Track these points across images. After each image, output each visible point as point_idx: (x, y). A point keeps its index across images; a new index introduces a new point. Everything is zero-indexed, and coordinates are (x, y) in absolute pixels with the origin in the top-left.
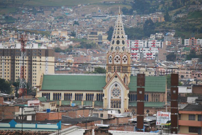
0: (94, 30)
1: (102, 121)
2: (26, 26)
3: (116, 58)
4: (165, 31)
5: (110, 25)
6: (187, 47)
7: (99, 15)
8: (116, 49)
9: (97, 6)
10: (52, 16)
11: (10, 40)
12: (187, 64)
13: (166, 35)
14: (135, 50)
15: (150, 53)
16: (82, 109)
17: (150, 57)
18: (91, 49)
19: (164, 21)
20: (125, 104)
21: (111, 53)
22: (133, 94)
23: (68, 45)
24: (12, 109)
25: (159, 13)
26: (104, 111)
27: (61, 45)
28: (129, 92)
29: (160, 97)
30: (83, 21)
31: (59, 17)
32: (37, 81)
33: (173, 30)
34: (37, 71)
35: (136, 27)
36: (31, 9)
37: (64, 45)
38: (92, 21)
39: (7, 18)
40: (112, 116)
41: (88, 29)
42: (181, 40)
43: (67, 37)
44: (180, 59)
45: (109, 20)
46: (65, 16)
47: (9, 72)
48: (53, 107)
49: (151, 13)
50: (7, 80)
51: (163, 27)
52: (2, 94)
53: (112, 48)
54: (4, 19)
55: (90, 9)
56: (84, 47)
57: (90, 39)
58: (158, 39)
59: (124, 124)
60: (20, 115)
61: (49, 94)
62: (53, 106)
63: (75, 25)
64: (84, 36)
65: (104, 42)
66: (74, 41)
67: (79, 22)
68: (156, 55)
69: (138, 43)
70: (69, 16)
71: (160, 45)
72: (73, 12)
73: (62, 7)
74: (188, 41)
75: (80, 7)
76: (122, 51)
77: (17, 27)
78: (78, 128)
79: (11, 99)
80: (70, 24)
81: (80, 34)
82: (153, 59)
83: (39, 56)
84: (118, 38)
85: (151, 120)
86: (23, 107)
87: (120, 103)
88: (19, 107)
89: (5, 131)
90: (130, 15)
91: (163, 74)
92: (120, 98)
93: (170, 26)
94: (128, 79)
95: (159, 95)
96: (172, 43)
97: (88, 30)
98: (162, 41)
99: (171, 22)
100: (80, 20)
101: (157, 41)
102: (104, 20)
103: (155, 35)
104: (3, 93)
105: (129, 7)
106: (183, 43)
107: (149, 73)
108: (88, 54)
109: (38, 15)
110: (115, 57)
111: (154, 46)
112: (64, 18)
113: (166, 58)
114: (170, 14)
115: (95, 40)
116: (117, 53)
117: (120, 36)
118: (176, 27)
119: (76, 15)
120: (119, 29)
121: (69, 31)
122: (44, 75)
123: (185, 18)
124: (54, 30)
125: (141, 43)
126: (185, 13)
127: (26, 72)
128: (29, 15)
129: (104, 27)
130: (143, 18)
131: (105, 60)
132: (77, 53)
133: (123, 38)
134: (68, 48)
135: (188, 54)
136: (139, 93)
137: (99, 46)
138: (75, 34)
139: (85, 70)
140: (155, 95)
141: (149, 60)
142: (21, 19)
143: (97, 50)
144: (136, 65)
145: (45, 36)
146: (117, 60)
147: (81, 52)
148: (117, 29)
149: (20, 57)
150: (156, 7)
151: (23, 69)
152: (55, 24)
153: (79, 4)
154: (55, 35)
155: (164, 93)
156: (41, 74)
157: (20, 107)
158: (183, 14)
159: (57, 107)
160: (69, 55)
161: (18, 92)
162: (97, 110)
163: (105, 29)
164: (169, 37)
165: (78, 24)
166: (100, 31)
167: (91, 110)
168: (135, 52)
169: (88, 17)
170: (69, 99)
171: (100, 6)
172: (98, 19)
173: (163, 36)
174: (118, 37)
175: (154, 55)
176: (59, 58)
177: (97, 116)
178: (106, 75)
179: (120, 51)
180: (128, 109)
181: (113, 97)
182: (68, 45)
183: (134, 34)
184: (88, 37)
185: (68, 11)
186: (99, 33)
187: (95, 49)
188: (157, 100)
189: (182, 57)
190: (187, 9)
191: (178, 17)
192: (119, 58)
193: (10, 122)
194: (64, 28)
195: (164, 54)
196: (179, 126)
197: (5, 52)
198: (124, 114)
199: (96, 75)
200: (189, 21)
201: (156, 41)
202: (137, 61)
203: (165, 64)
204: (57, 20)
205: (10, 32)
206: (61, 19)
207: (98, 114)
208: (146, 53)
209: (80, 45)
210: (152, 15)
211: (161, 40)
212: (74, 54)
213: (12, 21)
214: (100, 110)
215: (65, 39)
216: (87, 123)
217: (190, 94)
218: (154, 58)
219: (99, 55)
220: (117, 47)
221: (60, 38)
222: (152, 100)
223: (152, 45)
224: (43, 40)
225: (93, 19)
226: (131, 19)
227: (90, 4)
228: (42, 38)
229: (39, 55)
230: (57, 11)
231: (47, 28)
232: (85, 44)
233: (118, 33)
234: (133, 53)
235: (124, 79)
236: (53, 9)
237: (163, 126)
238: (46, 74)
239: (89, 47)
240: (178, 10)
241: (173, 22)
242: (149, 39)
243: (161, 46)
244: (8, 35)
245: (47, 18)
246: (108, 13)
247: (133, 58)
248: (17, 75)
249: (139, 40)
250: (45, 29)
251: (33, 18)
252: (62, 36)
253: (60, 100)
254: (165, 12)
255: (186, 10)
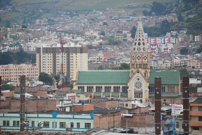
0: (120, 29)
1: (127, 110)
2: (65, 27)
3: (138, 57)
4: (179, 29)
5: (134, 25)
6: (197, 42)
7: (124, 17)
8: (138, 50)
9: (122, 9)
10: (86, 18)
11: (52, 39)
12: (197, 57)
13: (180, 32)
14: (154, 46)
15: (166, 48)
16: (110, 100)
17: (166, 52)
18: (118, 46)
19: (178, 21)
20: (146, 95)
21: (133, 53)
22: (152, 86)
23: (99, 42)
24: (54, 102)
25: (173, 14)
26: (129, 102)
27: (93, 43)
28: (149, 85)
29: (174, 88)
30: (111, 22)
31: (91, 19)
32: (74, 77)
33: (185, 29)
34: (73, 65)
35: (154, 26)
36: (69, 13)
37: (95, 43)
38: (118, 22)
39: (49, 20)
40: (135, 105)
41: (115, 28)
42: (192, 37)
43: (98, 36)
44: (191, 53)
45: (132, 21)
46: (96, 18)
47: (51, 61)
48: (86, 98)
49: (167, 14)
50: (50, 74)
51: (177, 26)
52: (46, 86)
53: (134, 49)
54: (47, 22)
55: (117, 11)
56: (111, 44)
57: (116, 37)
58: (173, 36)
59: (145, 113)
60: (60, 107)
61: (84, 87)
62: (86, 97)
63: (104, 25)
64: (112, 35)
65: (128, 40)
66: (103, 39)
67: (107, 23)
68: (172, 50)
69: (156, 40)
70: (99, 18)
71: (174, 41)
72: (102, 15)
73: (94, 11)
74: (198, 37)
75: (108, 10)
76: (143, 51)
77: (58, 28)
78: (106, 132)
79: (53, 92)
80: (101, 24)
81: (109, 33)
82: (169, 53)
83: (75, 53)
84: (139, 41)
85: (168, 109)
86: (62, 101)
87: (142, 94)
88: (59, 100)
89: (47, 133)
90: (150, 16)
91: (178, 66)
92: (142, 89)
93: (183, 25)
94: (148, 74)
95: (174, 87)
96: (184, 39)
97: (115, 29)
98: (176, 38)
99: (184, 22)
100: (109, 21)
101: (172, 38)
102: (129, 21)
103: (170, 33)
104: (47, 85)
105: (148, 10)
106: (194, 39)
107: (166, 65)
108: (115, 50)
109: (74, 18)
111: (169, 42)
112: (95, 19)
113: (180, 52)
114: (182, 15)
115: (121, 38)
116: (139, 53)
117: (140, 39)
118: (188, 26)
119: (105, 17)
120: (140, 33)
121: (100, 30)
122: (79, 71)
123: (195, 18)
124: (87, 30)
125: (159, 40)
126: (195, 14)
127: (65, 69)
128: (67, 18)
129: (128, 27)
130: (160, 19)
131: (129, 54)
132: (107, 49)
133: (144, 40)
134: (99, 45)
135: (198, 48)
136: (156, 93)
137: (124, 43)
138: (105, 33)
139: (113, 63)
140: (170, 87)
141: (166, 54)
142: (60, 21)
143: (122, 46)
144: (155, 58)
145: (80, 35)
147: (109, 48)
148: (138, 33)
149: (60, 54)
150: (171, 9)
151: (62, 69)
152: (88, 25)
153: (108, 8)
154: (88, 35)
155: (178, 85)
156: (77, 71)
157: (60, 101)
158: (193, 15)
159: (90, 98)
160: (100, 51)
161: (59, 84)
162: (122, 101)
163: (129, 28)
164: (182, 34)
165: (107, 25)
166: (125, 30)
167: (118, 101)
168: (154, 47)
169: (115, 18)
170: (100, 91)
171: (125, 9)
172: (123, 20)
173: (177, 34)
174: (139, 40)
175: (170, 50)
176: (92, 54)
177: (123, 106)
178: (130, 71)
179: (141, 51)
180: (148, 99)
181: (136, 89)
182: (99, 42)
183: (153, 32)
184: (115, 35)
185: (98, 14)
186: (124, 32)
187: (121, 45)
188: (172, 91)
189: (193, 51)
190: (197, 11)
191: (189, 18)
192: (140, 57)
193: (52, 114)
194: (96, 28)
195: (178, 49)
196: (191, 116)
197: (48, 50)
198: (145, 104)
199: (122, 71)
200: (198, 21)
201: (171, 38)
202: (155, 55)
203: (178, 57)
204: (90, 21)
205: (52, 33)
206: (93, 21)
207: (124, 104)
208: (163, 48)
209: (108, 43)
210: (168, 16)
211: (175, 37)
212: (104, 50)
213: (53, 23)
214: (125, 101)
215: (96, 37)
216: (115, 114)
217: (200, 84)
218: (169, 52)
219: (124, 51)
220: (139, 48)
221: (92, 37)
222: (168, 91)
223: (168, 41)
224: (79, 39)
225: (119, 20)
226: (151, 19)
227: (117, 8)
228: (77, 37)
229: (75, 52)
230: (90, 14)
231: (82, 28)
232: (112, 41)
233: (139, 36)
234: (152, 48)
235: (145, 74)
236: (86, 12)
237: (177, 116)
238: (81, 71)
239: (116, 43)
240: (189, 12)
241: (185, 22)
242: (165, 36)
243: (176, 42)
244: (50, 36)
245: (81, 20)
246: (131, 15)
247: (152, 52)
248: (58, 69)
249: (157, 37)
250: (80, 29)
251: (70, 20)
252: (93, 35)
253: (93, 92)
254: (178, 13)
255: (196, 11)
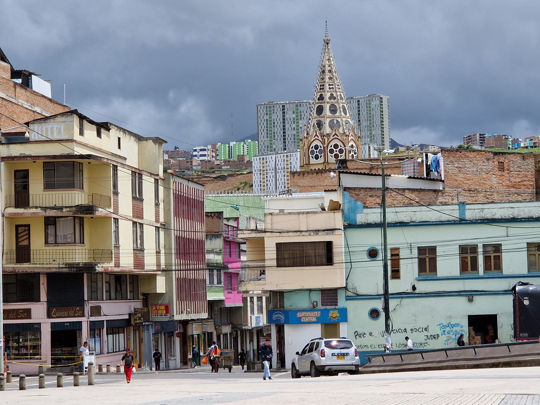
110: (331, 146)
116: (336, 136)
146: (335, 153)
